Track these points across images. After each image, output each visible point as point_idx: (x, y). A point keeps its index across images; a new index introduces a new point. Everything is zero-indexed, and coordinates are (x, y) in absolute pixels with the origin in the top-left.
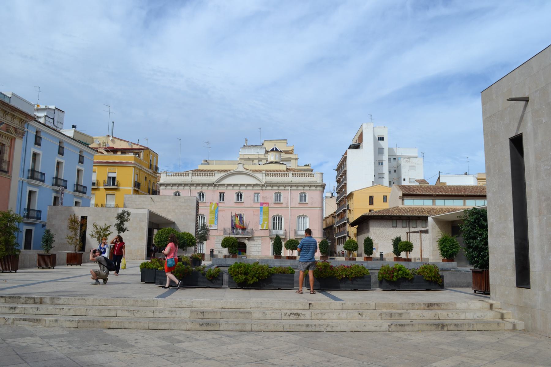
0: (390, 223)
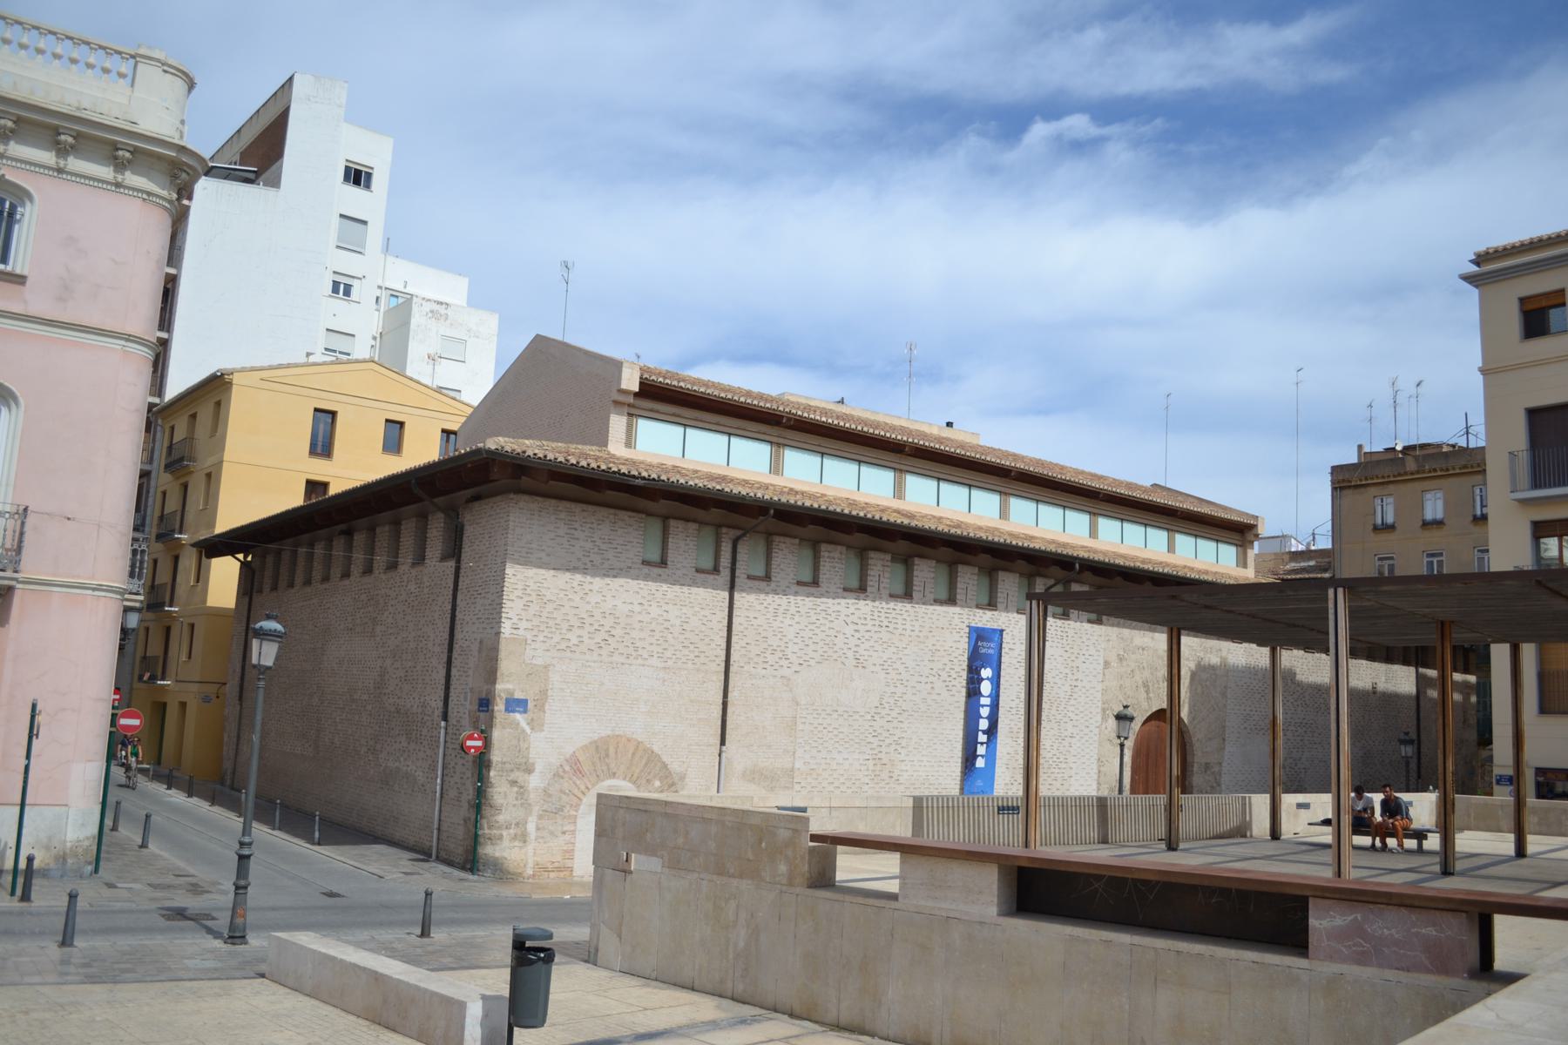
0: (633, 536)
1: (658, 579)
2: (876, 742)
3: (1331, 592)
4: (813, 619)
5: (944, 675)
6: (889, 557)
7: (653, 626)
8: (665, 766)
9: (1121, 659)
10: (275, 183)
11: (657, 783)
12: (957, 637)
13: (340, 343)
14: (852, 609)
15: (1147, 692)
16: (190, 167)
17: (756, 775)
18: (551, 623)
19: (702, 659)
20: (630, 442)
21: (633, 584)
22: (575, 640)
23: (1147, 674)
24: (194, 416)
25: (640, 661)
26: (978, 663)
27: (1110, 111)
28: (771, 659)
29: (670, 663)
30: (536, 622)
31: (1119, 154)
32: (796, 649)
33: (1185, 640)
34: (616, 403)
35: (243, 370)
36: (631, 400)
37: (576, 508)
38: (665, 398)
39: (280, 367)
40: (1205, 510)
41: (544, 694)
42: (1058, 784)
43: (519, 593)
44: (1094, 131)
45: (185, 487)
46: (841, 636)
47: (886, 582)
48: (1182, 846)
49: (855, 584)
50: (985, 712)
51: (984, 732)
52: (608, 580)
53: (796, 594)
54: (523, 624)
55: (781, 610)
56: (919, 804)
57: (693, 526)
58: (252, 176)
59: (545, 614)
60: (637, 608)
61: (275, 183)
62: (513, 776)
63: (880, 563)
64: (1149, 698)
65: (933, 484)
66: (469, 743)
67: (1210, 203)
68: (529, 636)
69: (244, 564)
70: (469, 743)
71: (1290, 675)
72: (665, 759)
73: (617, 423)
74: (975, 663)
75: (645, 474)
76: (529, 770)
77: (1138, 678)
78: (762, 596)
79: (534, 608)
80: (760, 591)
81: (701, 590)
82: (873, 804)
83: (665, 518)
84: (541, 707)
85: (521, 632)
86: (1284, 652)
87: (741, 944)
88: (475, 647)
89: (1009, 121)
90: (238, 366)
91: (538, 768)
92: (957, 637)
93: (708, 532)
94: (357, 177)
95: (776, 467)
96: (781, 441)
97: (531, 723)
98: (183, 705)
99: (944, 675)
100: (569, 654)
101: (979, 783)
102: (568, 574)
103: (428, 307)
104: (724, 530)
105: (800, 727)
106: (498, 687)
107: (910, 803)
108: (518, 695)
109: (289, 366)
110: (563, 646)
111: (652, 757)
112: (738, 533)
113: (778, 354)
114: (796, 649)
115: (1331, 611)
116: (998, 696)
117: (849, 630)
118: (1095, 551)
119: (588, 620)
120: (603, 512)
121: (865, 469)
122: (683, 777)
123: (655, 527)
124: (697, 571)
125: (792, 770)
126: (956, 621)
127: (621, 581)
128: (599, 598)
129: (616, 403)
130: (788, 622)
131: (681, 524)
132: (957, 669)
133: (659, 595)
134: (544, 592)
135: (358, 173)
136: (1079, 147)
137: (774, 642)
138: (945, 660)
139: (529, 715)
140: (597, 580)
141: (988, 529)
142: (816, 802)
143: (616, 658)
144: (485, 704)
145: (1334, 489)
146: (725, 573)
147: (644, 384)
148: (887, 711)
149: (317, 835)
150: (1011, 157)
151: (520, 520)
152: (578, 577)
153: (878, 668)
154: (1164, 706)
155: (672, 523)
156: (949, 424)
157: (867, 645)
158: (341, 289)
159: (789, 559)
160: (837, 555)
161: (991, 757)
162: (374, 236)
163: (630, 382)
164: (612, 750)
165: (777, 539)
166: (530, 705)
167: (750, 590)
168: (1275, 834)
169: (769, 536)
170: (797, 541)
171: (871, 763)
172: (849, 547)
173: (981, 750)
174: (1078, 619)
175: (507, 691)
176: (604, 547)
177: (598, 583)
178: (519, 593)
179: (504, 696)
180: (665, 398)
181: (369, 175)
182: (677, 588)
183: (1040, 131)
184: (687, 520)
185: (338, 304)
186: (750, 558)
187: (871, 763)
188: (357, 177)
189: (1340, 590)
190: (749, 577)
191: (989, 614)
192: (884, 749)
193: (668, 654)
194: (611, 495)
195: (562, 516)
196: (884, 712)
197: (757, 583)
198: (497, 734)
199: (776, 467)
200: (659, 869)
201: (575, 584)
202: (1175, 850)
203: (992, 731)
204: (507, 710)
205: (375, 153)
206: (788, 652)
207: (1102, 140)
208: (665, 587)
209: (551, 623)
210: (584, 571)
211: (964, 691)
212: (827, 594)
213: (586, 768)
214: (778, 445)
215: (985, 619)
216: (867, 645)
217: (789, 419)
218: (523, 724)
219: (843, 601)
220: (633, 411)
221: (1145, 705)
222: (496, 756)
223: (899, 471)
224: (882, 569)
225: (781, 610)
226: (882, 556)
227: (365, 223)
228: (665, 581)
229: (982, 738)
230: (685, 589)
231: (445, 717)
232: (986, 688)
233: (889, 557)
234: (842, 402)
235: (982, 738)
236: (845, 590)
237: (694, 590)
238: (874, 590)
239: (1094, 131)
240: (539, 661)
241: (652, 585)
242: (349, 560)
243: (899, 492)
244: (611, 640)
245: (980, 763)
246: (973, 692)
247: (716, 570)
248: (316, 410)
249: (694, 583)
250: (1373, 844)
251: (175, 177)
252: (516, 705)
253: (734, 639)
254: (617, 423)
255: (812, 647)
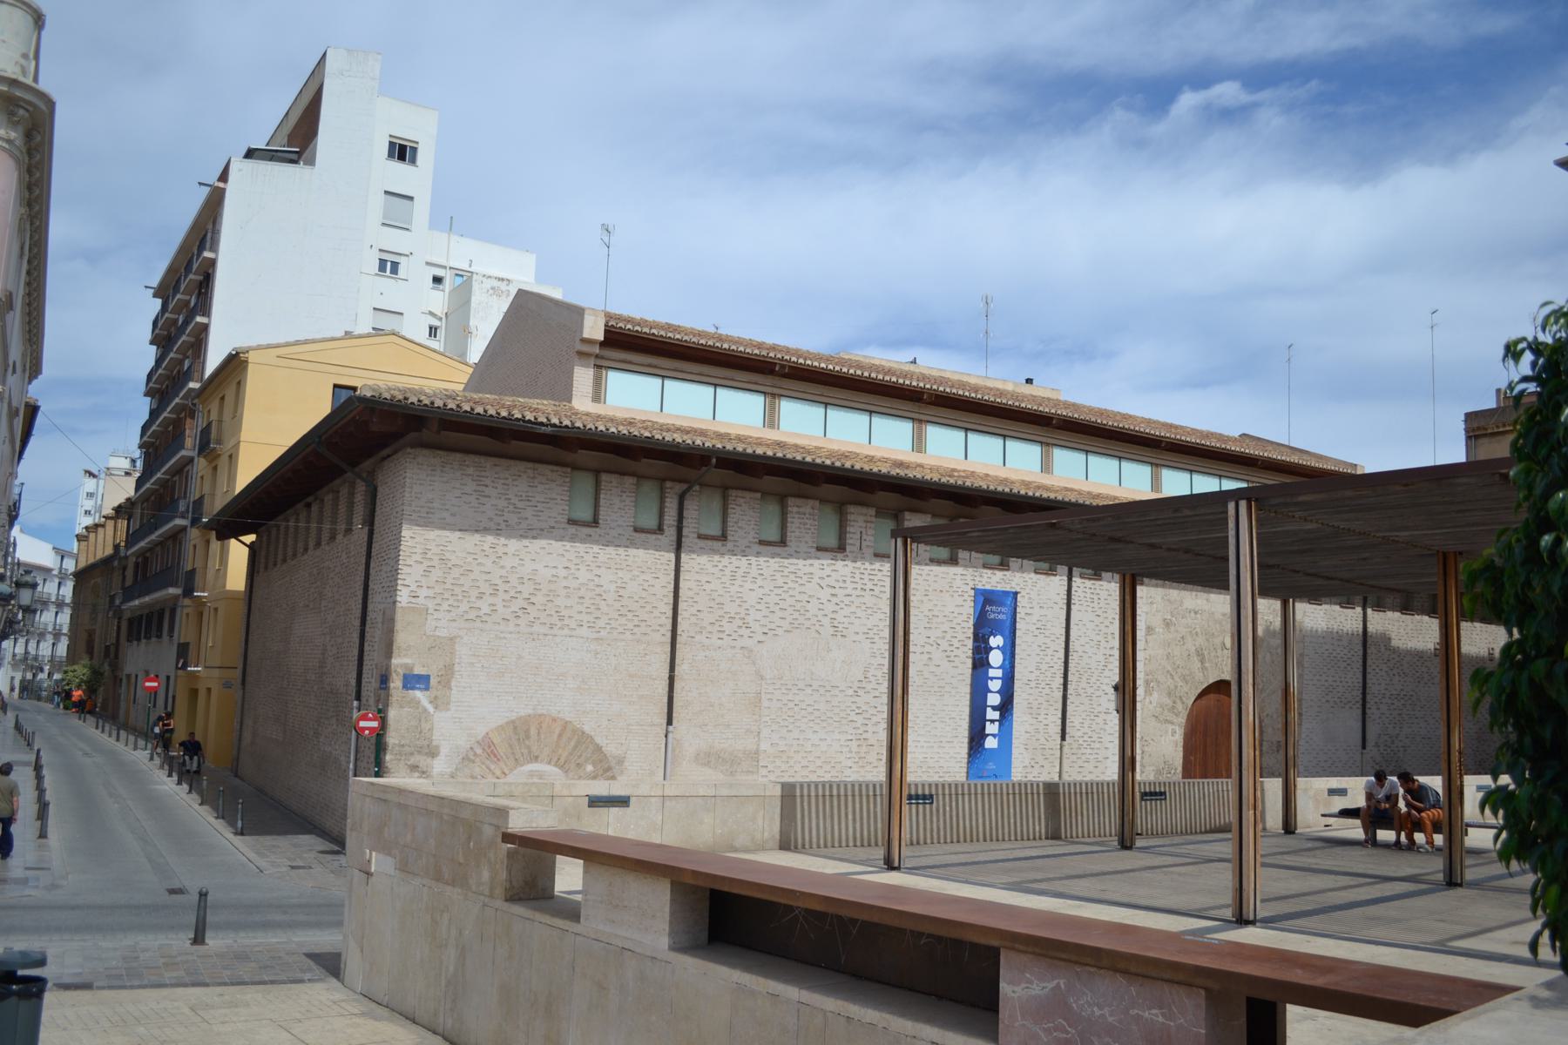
0: (552, 493)
1: (587, 539)
2: (860, 720)
3: (1231, 506)
4: (780, 582)
5: (944, 645)
6: (872, 511)
7: (582, 592)
8: (599, 749)
9: (1167, 624)
10: (311, 162)
11: (590, 768)
12: (959, 601)
13: (387, 323)
14: (828, 571)
15: (1202, 662)
16: (29, 103)
17: (707, 758)
18: (457, 590)
19: (643, 629)
20: (598, 395)
21: (557, 546)
22: (486, 609)
23: (1200, 640)
24: (223, 398)
25: (566, 631)
26: (986, 630)
27: (1260, 77)
28: (728, 628)
29: (603, 633)
30: (438, 589)
31: (1271, 120)
32: (759, 616)
33: (1142, 591)
34: (581, 354)
35: (259, 348)
36: (597, 350)
37: (488, 462)
38: (631, 345)
39: (297, 343)
40: (1295, 459)
41: (449, 671)
42: (1090, 766)
43: (418, 557)
44: (1245, 98)
45: (215, 468)
46: (814, 601)
47: (869, 540)
48: (1139, 843)
49: (832, 542)
50: (995, 685)
51: (994, 708)
52: (526, 542)
53: (758, 554)
54: (423, 593)
55: (740, 572)
56: (789, 793)
57: (630, 481)
58: (294, 157)
59: (449, 580)
60: (563, 573)
61: (311, 162)
62: (412, 761)
63: (861, 518)
64: (1204, 668)
65: (1081, 457)
66: (362, 724)
67: (1368, 164)
68: (431, 605)
69: (251, 546)
70: (362, 724)
71: (1385, 639)
72: (598, 740)
73: (583, 377)
74: (982, 630)
75: (555, 421)
76: (433, 753)
77: (1190, 646)
78: (717, 558)
79: (436, 574)
80: (714, 551)
81: (641, 552)
82: (725, 792)
83: (597, 472)
84: (446, 684)
85: (421, 600)
86: (1298, 605)
87: (451, 968)
88: (380, 620)
89: (1155, 93)
90: (253, 343)
91: (444, 750)
92: (959, 601)
93: (649, 488)
94: (402, 152)
95: (771, 419)
96: (776, 391)
97: (434, 701)
98: (209, 690)
99: (944, 645)
100: (478, 624)
101: (991, 766)
102: (477, 536)
103: (489, 283)
104: (668, 484)
105: (765, 703)
106: (394, 661)
107: (778, 791)
108: (418, 670)
109: (306, 342)
110: (472, 615)
111: (583, 738)
112: (685, 486)
113: (933, 341)
114: (759, 616)
115: (1232, 541)
116: (1013, 667)
117: (824, 594)
118: (1047, 489)
119: (502, 587)
120: (522, 465)
121: (1093, 459)
122: (621, 761)
123: (773, 508)
124: (636, 530)
125: (757, 752)
126: (958, 582)
127: (543, 542)
128: (516, 562)
129: (581, 354)
130: (748, 585)
131: (614, 478)
132: (961, 636)
133: (589, 558)
134: (448, 555)
135: (403, 149)
136: (1228, 115)
137: (732, 608)
138: (946, 627)
139: (432, 693)
140: (513, 541)
141: (1027, 484)
142: (644, 790)
143: (537, 628)
144: (384, 680)
145: (1468, 438)
146: (670, 532)
147: (609, 332)
148: (873, 685)
149: (239, 824)
150: (1159, 129)
151: (415, 480)
152: (490, 539)
153: (861, 637)
154: (1227, 674)
155: (604, 477)
156: (1029, 381)
157: (847, 611)
158: (389, 266)
159: (748, 515)
160: (808, 510)
161: (1005, 736)
162: (421, 211)
163: (594, 330)
164: (533, 731)
165: (733, 493)
166: (433, 681)
167: (702, 551)
168: (1289, 827)
169: (725, 490)
170: (758, 495)
171: (855, 744)
172: (823, 501)
173: (991, 728)
174: (1021, 569)
175: (405, 666)
176: (520, 505)
177: (514, 545)
178: (418, 557)
179: (401, 672)
180: (631, 345)
181: (414, 150)
182: (611, 550)
183: (1188, 100)
184: (623, 474)
185: (386, 283)
186: (701, 514)
187: (855, 744)
188: (402, 152)
189: (1243, 504)
190: (700, 537)
191: (999, 574)
192: (870, 728)
193: (601, 623)
194: (516, 445)
195: (470, 471)
196: (869, 687)
197: (710, 543)
198: (392, 714)
199: (919, 444)
200: (392, 871)
201: (486, 547)
202: (1129, 848)
203: (1006, 707)
204: (405, 687)
205: (418, 128)
206: (749, 619)
207: (1256, 105)
208: (596, 548)
209: (457, 590)
210: (498, 532)
211: (969, 663)
212: (797, 554)
213: (502, 750)
214: (773, 396)
215: (995, 580)
216: (847, 611)
217: (783, 366)
218: (425, 703)
219: (817, 562)
220: (599, 362)
221: (1199, 676)
222: (392, 739)
223: (919, 421)
224: (806, 519)
225: (740, 572)
226: (864, 510)
227: (411, 198)
228: (597, 542)
229: (992, 714)
230: (621, 551)
231: (358, 698)
232: (996, 658)
233: (872, 511)
234: (914, 362)
235: (992, 714)
236: (819, 549)
237: (632, 551)
238: (856, 549)
239: (1245, 98)
240: (443, 633)
241: (581, 547)
242: (320, 530)
243: (1046, 466)
244: (530, 609)
245: (991, 743)
246: (980, 662)
247: (660, 529)
248: (335, 386)
249: (631, 544)
250: (1398, 842)
251: (11, 114)
252: (415, 681)
253: (682, 606)
254: (583, 377)
255: (779, 614)
